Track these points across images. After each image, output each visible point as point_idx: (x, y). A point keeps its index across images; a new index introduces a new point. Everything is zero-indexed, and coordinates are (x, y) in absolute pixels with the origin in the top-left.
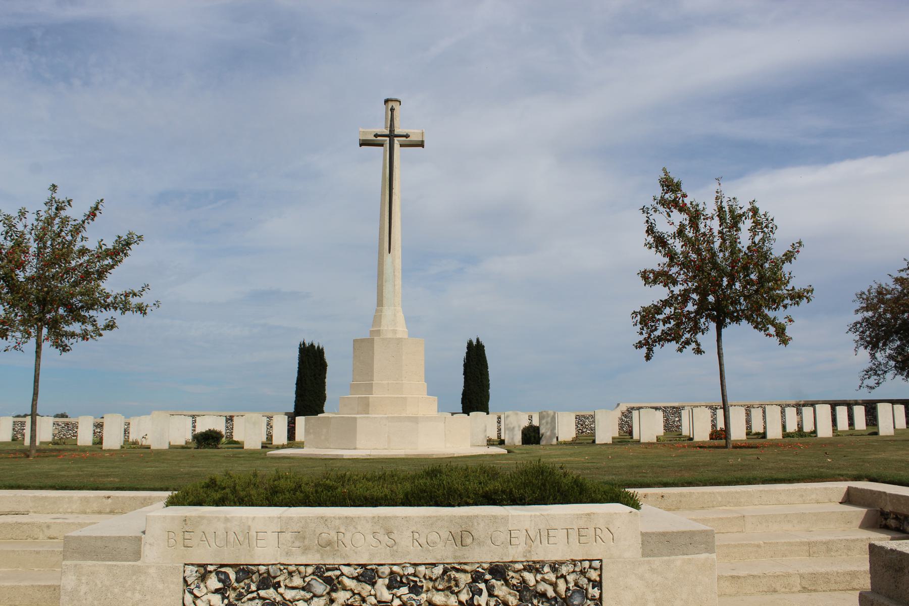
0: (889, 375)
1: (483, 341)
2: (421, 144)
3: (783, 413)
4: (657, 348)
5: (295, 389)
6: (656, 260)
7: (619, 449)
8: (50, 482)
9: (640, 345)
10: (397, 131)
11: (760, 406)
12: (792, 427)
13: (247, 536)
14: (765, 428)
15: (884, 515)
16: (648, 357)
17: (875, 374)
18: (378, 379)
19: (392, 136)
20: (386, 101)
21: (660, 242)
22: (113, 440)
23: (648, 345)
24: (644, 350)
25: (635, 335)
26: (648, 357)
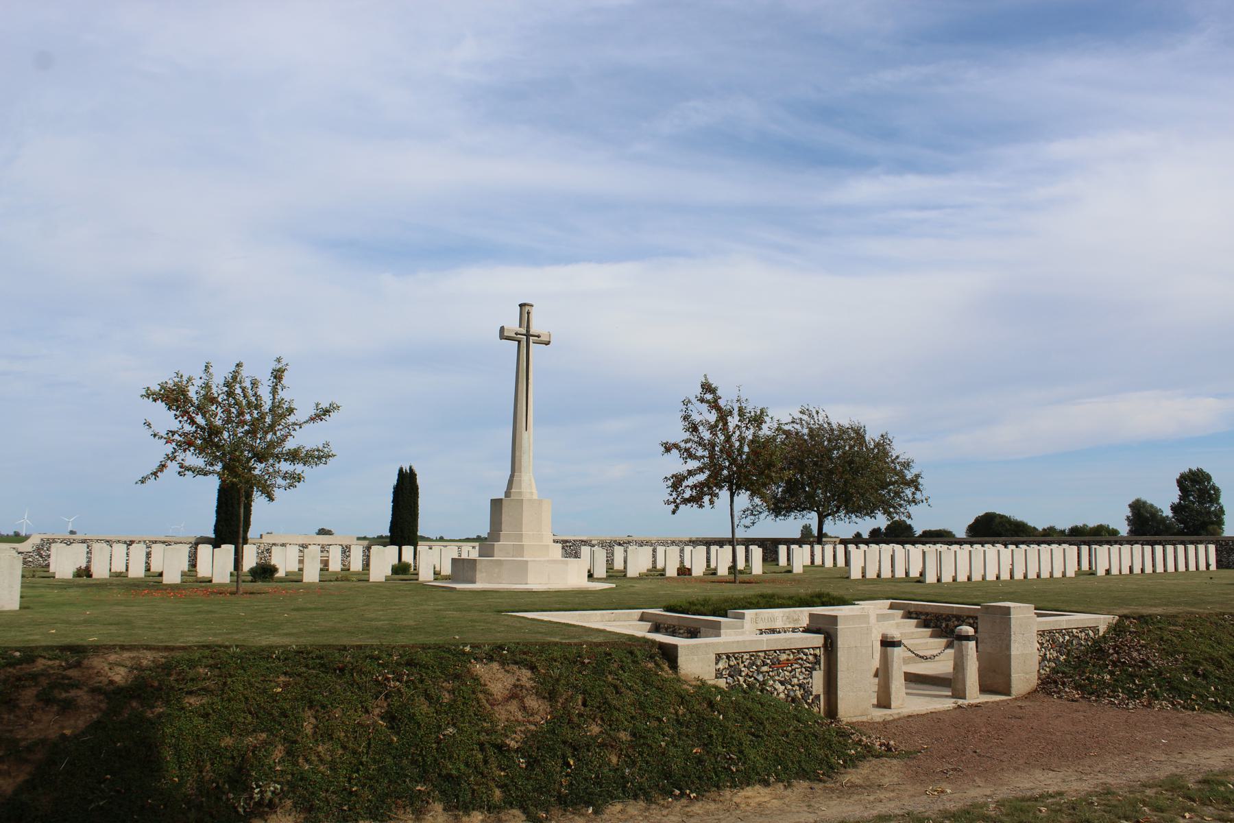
0: (762, 516)
1: (417, 471)
2: (548, 343)
3: (682, 551)
4: (682, 507)
5: (214, 523)
6: (678, 434)
7: (24, 612)
8: (570, 606)
9: (668, 503)
10: (534, 330)
11: (602, 544)
12: (335, 566)
13: (773, 619)
14: (89, 562)
15: (910, 613)
16: (674, 512)
17: (752, 514)
18: (526, 531)
19: (528, 335)
20: (521, 306)
21: (694, 428)
22: (947, 578)
23: (174, 397)
24: (673, 506)
25: (665, 493)
26: (674, 512)
